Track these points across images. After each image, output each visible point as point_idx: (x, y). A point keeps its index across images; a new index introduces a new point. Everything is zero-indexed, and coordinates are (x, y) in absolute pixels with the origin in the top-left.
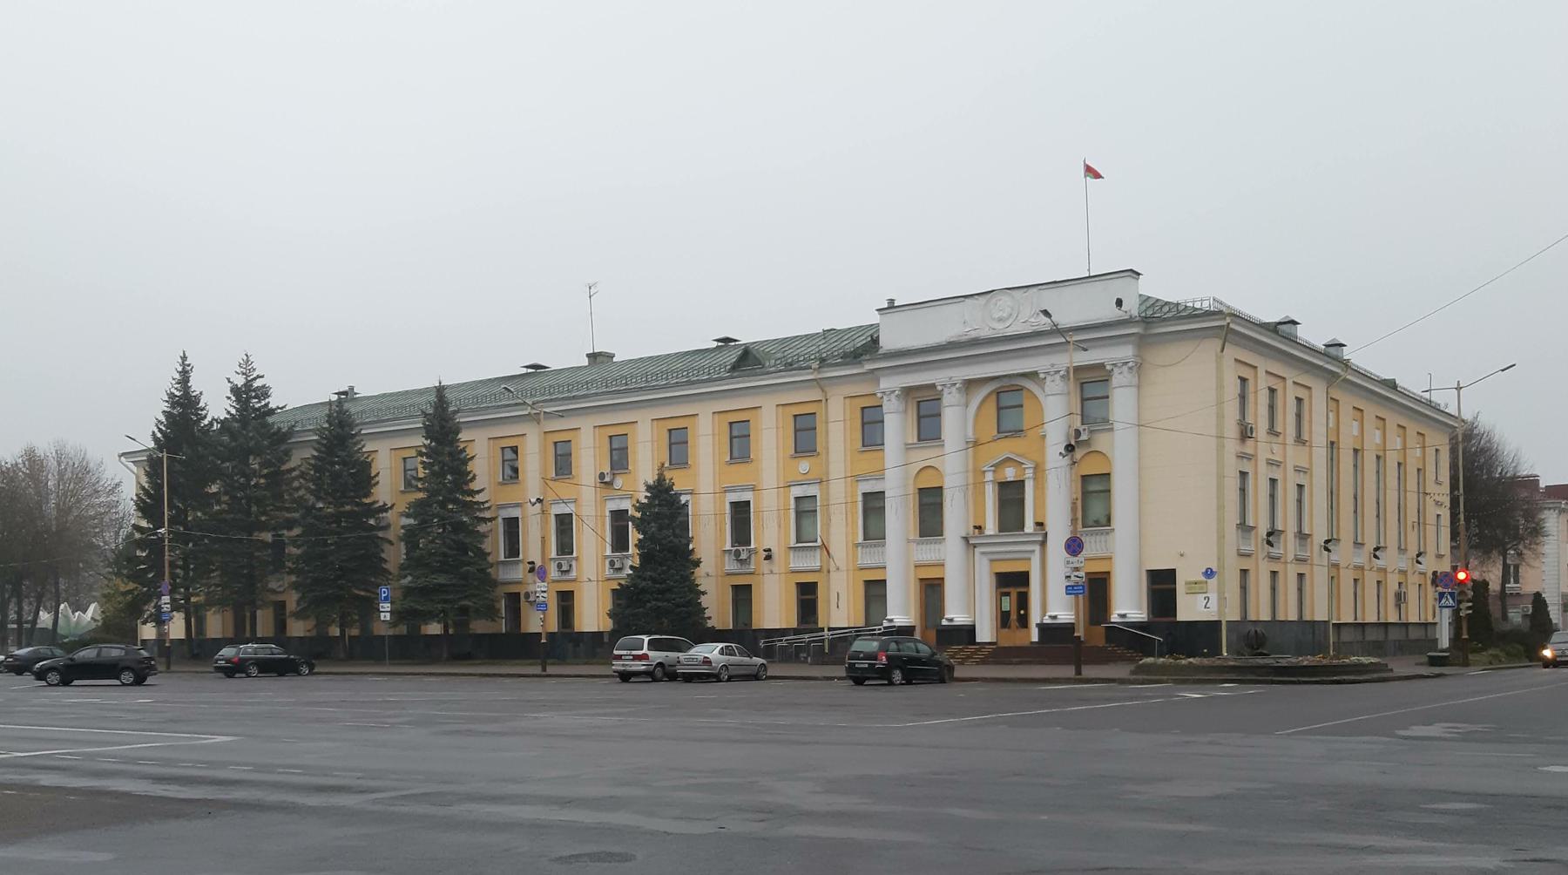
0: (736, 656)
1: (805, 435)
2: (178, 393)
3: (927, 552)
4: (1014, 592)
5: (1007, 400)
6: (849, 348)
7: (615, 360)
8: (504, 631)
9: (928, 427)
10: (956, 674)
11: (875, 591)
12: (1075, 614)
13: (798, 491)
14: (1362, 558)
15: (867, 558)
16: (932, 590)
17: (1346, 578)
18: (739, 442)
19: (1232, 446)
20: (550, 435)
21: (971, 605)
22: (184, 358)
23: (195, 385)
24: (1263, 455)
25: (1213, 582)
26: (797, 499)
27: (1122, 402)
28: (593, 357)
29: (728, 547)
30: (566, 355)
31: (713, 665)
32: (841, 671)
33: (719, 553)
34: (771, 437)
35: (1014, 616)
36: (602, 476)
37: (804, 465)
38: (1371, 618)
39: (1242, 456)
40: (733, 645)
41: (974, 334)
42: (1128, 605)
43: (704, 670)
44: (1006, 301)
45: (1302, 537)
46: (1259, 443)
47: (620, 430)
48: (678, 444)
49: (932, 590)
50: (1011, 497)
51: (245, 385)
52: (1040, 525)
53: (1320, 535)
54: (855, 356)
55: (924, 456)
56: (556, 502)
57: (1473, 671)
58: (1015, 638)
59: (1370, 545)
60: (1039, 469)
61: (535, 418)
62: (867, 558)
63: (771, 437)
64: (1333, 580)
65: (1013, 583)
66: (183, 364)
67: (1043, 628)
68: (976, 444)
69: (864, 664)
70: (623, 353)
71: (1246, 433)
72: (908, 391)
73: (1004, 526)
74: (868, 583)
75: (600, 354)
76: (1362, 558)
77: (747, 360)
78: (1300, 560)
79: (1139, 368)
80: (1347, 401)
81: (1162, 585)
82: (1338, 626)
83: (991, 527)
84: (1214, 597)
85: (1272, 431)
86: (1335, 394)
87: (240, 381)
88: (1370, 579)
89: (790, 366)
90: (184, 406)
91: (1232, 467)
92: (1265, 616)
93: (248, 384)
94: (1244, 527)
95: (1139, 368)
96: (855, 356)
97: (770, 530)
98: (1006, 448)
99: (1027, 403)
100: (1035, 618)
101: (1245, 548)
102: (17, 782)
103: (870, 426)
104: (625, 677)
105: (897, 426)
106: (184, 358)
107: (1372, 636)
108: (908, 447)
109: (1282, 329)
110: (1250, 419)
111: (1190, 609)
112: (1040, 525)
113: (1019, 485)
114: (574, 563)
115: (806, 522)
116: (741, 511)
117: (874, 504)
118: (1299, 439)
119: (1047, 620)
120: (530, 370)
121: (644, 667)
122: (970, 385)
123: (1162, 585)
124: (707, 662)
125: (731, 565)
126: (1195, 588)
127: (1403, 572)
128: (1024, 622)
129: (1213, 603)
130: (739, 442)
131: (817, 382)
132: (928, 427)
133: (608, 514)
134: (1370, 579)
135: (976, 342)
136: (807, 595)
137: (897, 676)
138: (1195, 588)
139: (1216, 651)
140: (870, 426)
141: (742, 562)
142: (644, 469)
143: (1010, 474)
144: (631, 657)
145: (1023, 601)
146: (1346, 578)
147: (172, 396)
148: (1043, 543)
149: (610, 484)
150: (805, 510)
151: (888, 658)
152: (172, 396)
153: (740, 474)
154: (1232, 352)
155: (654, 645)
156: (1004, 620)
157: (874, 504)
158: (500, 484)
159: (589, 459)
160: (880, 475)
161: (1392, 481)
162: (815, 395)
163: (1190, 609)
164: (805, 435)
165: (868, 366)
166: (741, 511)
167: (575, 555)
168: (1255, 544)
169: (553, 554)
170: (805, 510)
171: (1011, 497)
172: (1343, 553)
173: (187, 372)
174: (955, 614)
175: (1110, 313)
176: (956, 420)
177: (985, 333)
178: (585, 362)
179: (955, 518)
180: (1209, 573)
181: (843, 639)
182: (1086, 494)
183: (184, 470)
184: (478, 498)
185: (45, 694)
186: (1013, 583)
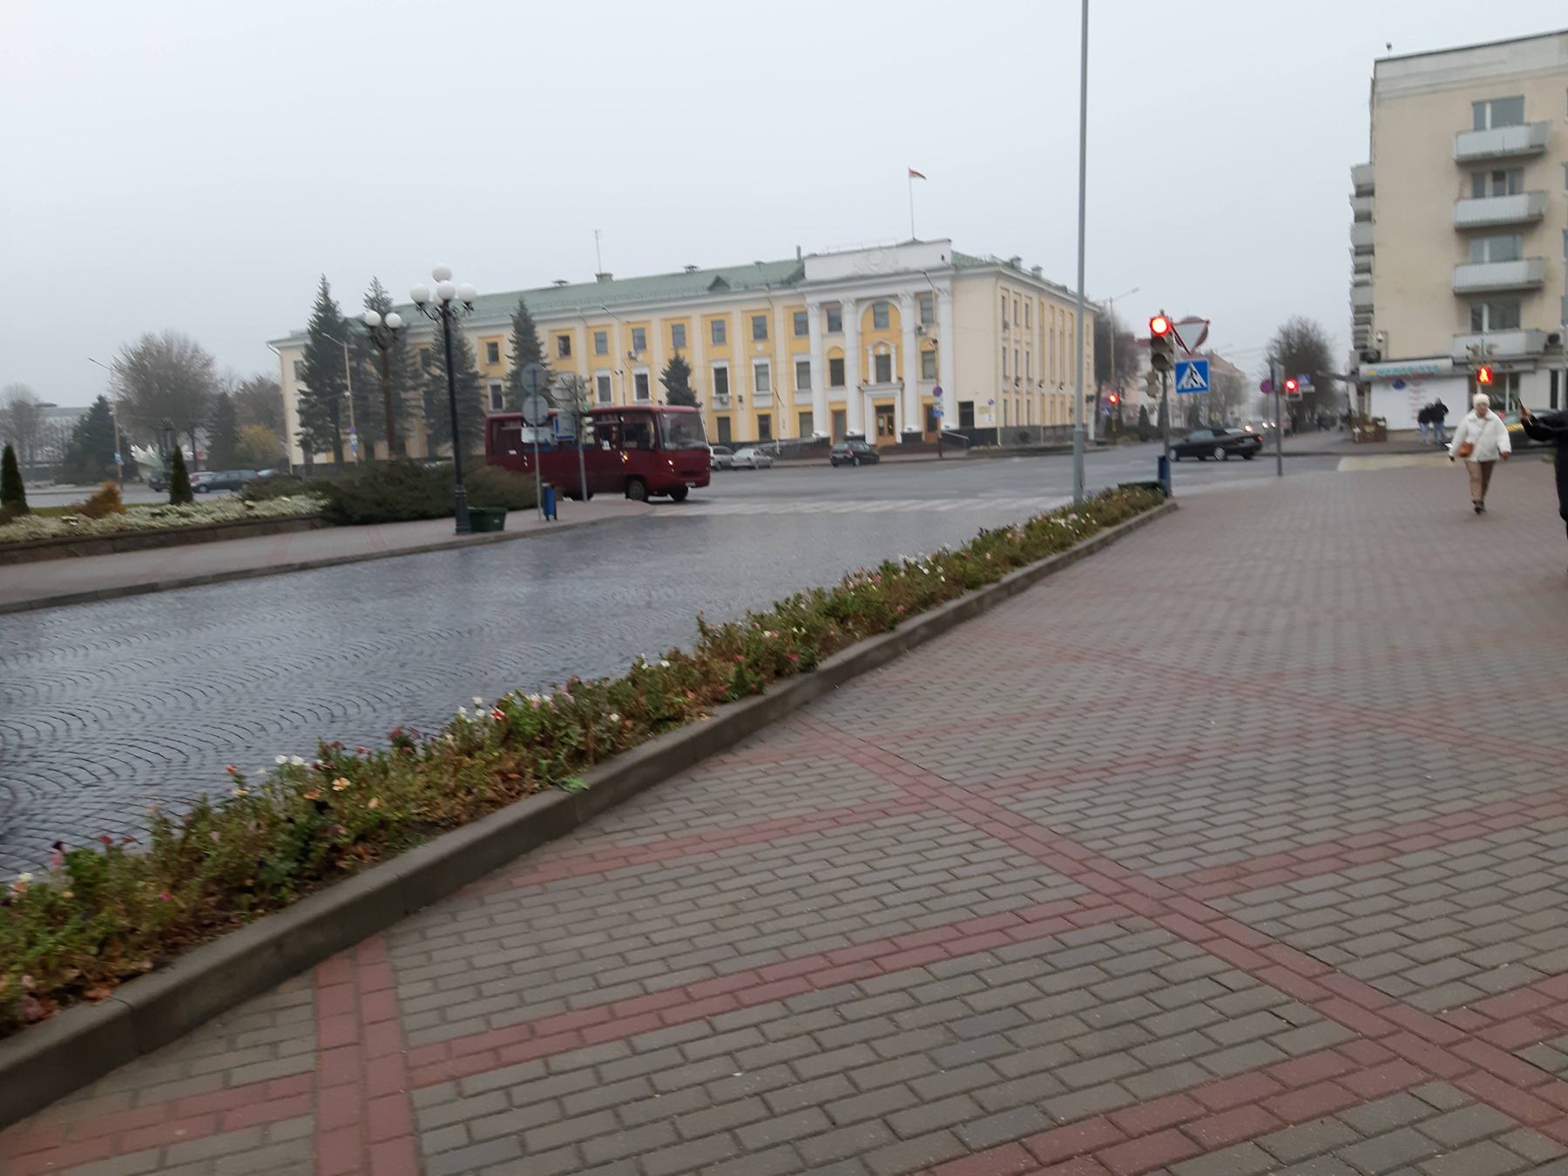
1: (760, 331)
3: (837, 395)
4: (885, 416)
5: (879, 309)
6: (785, 277)
9: (835, 325)
10: (688, 498)
11: (806, 418)
13: (757, 362)
14: (1054, 390)
15: (801, 399)
16: (839, 417)
17: (1048, 400)
18: (719, 332)
19: (1000, 334)
21: (863, 425)
22: (324, 279)
23: (333, 297)
24: (1013, 337)
25: (993, 407)
26: (756, 367)
27: (943, 311)
28: (600, 276)
29: (714, 394)
30: (581, 275)
32: (828, 461)
34: (738, 330)
35: (886, 429)
36: (630, 353)
37: (760, 346)
38: (1059, 423)
39: (1004, 339)
41: (861, 273)
42: (949, 421)
43: (748, 464)
44: (879, 254)
45: (1029, 380)
48: (679, 335)
49: (839, 417)
50: (883, 364)
52: (900, 379)
53: (1037, 380)
54: (789, 282)
55: (834, 340)
56: (598, 369)
57: (1120, 447)
58: (888, 441)
59: (1058, 381)
60: (898, 348)
61: (583, 319)
62: (801, 399)
63: (738, 330)
64: (1043, 402)
65: (885, 411)
66: (324, 283)
67: (904, 435)
68: (862, 334)
69: (840, 456)
70: (618, 276)
71: (1005, 326)
72: (822, 305)
73: (879, 380)
74: (801, 414)
76: (1054, 390)
77: (719, 283)
78: (1028, 393)
79: (952, 293)
80: (1047, 302)
81: (966, 410)
82: (1044, 428)
83: (872, 380)
84: (993, 415)
85: (1016, 324)
86: (1043, 300)
87: (372, 295)
88: (1058, 400)
89: (747, 288)
90: (327, 313)
91: (1001, 344)
92: (1026, 424)
94: (1006, 377)
95: (952, 293)
96: (789, 282)
97: (740, 383)
98: (880, 335)
99: (891, 312)
100: (898, 430)
101: (1006, 388)
102: (1391, 373)
103: (801, 327)
105: (817, 324)
106: (324, 279)
107: (1060, 432)
108: (823, 336)
109: (1013, 265)
110: (1007, 319)
111: (981, 421)
112: (900, 379)
113: (888, 357)
115: (761, 379)
116: (721, 374)
117: (803, 369)
118: (1027, 327)
119: (906, 431)
122: (859, 301)
123: (966, 410)
124: (749, 459)
125: (716, 405)
126: (983, 410)
127: (1053, 396)
128: (891, 432)
129: (993, 419)
130: (719, 332)
131: (769, 299)
132: (835, 325)
134: (1058, 400)
135: (863, 277)
136: (764, 423)
137: (857, 461)
138: (983, 410)
139: (995, 443)
140: (801, 327)
143: (882, 351)
144: (300, 504)
145: (891, 421)
146: (1048, 400)
147: (319, 304)
148: (902, 389)
150: (761, 371)
152: (319, 304)
153: (719, 351)
154: (1001, 283)
156: (880, 431)
157: (803, 369)
159: (619, 342)
160: (808, 352)
161: (1047, 339)
162: (766, 305)
163: (981, 421)
164: (760, 331)
165: (799, 290)
166: (721, 374)
168: (1010, 386)
170: (761, 371)
171: (883, 364)
172: (1048, 389)
174: (853, 429)
175: (937, 262)
176: (851, 320)
177: (867, 272)
178: (595, 280)
179: (852, 375)
180: (991, 402)
181: (824, 442)
182: (924, 361)
184: (549, 368)
186: (885, 411)
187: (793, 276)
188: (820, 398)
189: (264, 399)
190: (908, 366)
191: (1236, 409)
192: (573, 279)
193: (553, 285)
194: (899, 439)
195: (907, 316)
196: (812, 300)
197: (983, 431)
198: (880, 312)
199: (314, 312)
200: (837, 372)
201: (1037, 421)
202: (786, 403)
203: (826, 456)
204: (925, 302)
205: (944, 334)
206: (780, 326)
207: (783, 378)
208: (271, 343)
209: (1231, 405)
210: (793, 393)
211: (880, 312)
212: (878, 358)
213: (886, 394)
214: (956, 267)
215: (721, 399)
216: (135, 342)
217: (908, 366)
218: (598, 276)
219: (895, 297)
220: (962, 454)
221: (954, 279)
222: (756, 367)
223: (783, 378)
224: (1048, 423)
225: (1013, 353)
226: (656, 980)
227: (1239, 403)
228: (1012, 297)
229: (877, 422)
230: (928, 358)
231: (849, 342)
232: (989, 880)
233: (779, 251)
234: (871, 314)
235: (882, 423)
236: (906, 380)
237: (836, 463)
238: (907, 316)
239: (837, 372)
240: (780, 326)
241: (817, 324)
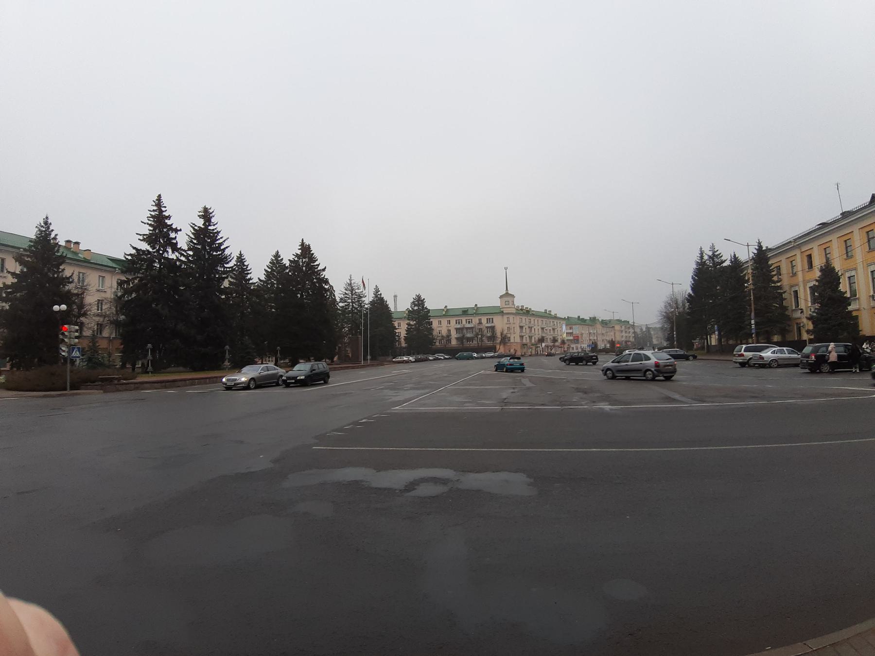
0: (785, 354)
2: (699, 261)
8: (796, 339)
12: (600, 349)
20: (804, 253)
22: (701, 248)
30: (832, 214)
31: (765, 359)
33: (869, 298)
40: (785, 348)
46: (749, 247)
51: (712, 255)
66: (701, 251)
93: (713, 254)
104: (743, 365)
120: (820, 226)
121: (741, 360)
142: (818, 261)
151: (816, 357)
155: (746, 350)
158: (792, 277)
167: (857, 297)
173: (702, 253)
183: (158, 352)
185: (411, 366)
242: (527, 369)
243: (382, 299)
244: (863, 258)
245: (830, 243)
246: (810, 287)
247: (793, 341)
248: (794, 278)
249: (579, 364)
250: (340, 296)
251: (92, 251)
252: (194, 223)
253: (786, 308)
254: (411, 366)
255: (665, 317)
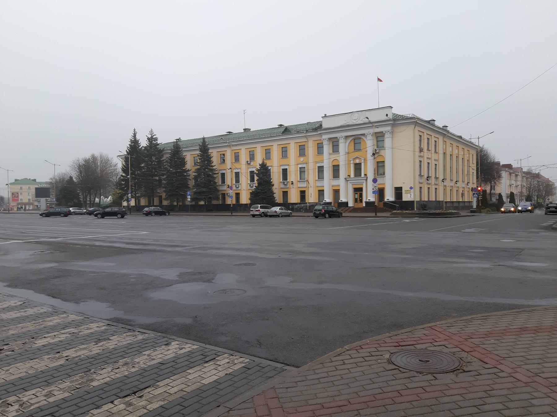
1: (302, 151)
2: (133, 140)
3: (335, 182)
4: (359, 193)
5: (357, 141)
7: (251, 130)
11: (321, 193)
13: (300, 166)
14: (452, 184)
15: (319, 184)
16: (336, 192)
17: (448, 189)
18: (284, 153)
19: (417, 154)
21: (347, 196)
22: (135, 130)
23: (138, 137)
24: (426, 156)
25: (412, 190)
27: (388, 142)
29: (281, 181)
30: (238, 129)
32: (312, 214)
34: (293, 151)
36: (247, 162)
37: (302, 159)
38: (455, 200)
39: (420, 156)
41: (348, 124)
43: (275, 214)
45: (436, 178)
47: (237, 151)
48: (268, 153)
49: (336, 192)
50: (358, 167)
51: (151, 137)
52: (366, 175)
53: (441, 178)
54: (316, 130)
55: (334, 156)
58: (359, 205)
60: (365, 160)
61: (229, 146)
62: (319, 184)
63: (293, 151)
65: (358, 191)
66: (134, 132)
67: (366, 203)
68: (348, 153)
70: (254, 128)
71: (421, 150)
72: (330, 139)
75: (247, 129)
76: (452, 184)
77: (287, 130)
79: (392, 133)
81: (398, 191)
82: (446, 202)
83: (352, 175)
84: (412, 194)
85: (428, 150)
87: (150, 136)
88: (455, 189)
89: (298, 132)
90: (134, 143)
92: (426, 199)
93: (152, 137)
94: (421, 175)
95: (392, 133)
96: (316, 130)
97: (293, 176)
98: (357, 154)
100: (364, 200)
101: (421, 181)
103: (320, 148)
105: (327, 148)
106: (135, 130)
108: (330, 154)
111: (406, 197)
112: (366, 175)
113: (360, 164)
114: (240, 185)
115: (302, 174)
116: (285, 172)
117: (321, 170)
119: (367, 201)
122: (347, 137)
123: (398, 191)
124: (276, 212)
125: (282, 186)
126: (407, 192)
127: (463, 188)
128: (361, 201)
129: (412, 196)
130: (284, 153)
132: (335, 148)
133: (249, 172)
134: (455, 189)
135: (348, 126)
136: (303, 194)
137: (327, 216)
140: (320, 148)
141: (285, 185)
142: (259, 159)
143: (357, 161)
145: (361, 195)
146: (448, 189)
147: (131, 140)
148: (366, 180)
149: (249, 164)
150: (302, 171)
152: (131, 140)
153: (284, 161)
154: (417, 128)
156: (356, 200)
157: (321, 170)
159: (244, 157)
162: (305, 140)
163: (406, 197)
164: (302, 151)
165: (319, 132)
167: (240, 183)
168: (424, 180)
169: (234, 183)
170: (302, 171)
171: (358, 167)
172: (448, 183)
174: (343, 199)
175: (384, 118)
176: (343, 147)
177: (351, 123)
178: (243, 131)
179: (343, 173)
180: (411, 188)
181: (312, 206)
184: (214, 168)
186: (358, 191)
187: (318, 128)
188: (327, 184)
189: (215, 180)
190: (369, 169)
191: (550, 197)
192: (235, 131)
193: (226, 133)
194: (364, 205)
195: (369, 144)
196: (325, 137)
197: (406, 202)
198: (357, 141)
199: (130, 143)
200: (336, 170)
201: (441, 199)
202: (312, 186)
203: (312, 212)
204: (379, 137)
205: (387, 155)
206: (311, 149)
207: (312, 175)
208: (118, 156)
209: (548, 196)
210: (330, 179)
211: (357, 141)
212: (356, 165)
213: (359, 182)
214: (394, 120)
215: (284, 183)
216: (86, 154)
217: (369, 169)
218: (244, 129)
219: (363, 135)
220: (387, 214)
221: (393, 126)
222: (377, 175)
223: (312, 175)
224: (448, 200)
225: (434, 167)
226: (331, 370)
227: (552, 195)
228: (425, 137)
229: (355, 196)
230: (380, 166)
231: (342, 159)
232: (427, 384)
233: (315, 118)
234: (352, 144)
235: (357, 196)
236: (368, 176)
237: (316, 216)
238: (369, 144)
239: (336, 170)
240: (311, 149)
241: (327, 148)
242: (22, 198)
243: (348, 202)
244: (313, 167)
245: (255, 148)
246: (235, 172)
247: (218, 205)
248: (223, 165)
249: (105, 217)
250: (488, 187)
251: (37, 181)
252: (51, 304)
253: (215, 183)
254: (66, 352)
255: (86, 161)
